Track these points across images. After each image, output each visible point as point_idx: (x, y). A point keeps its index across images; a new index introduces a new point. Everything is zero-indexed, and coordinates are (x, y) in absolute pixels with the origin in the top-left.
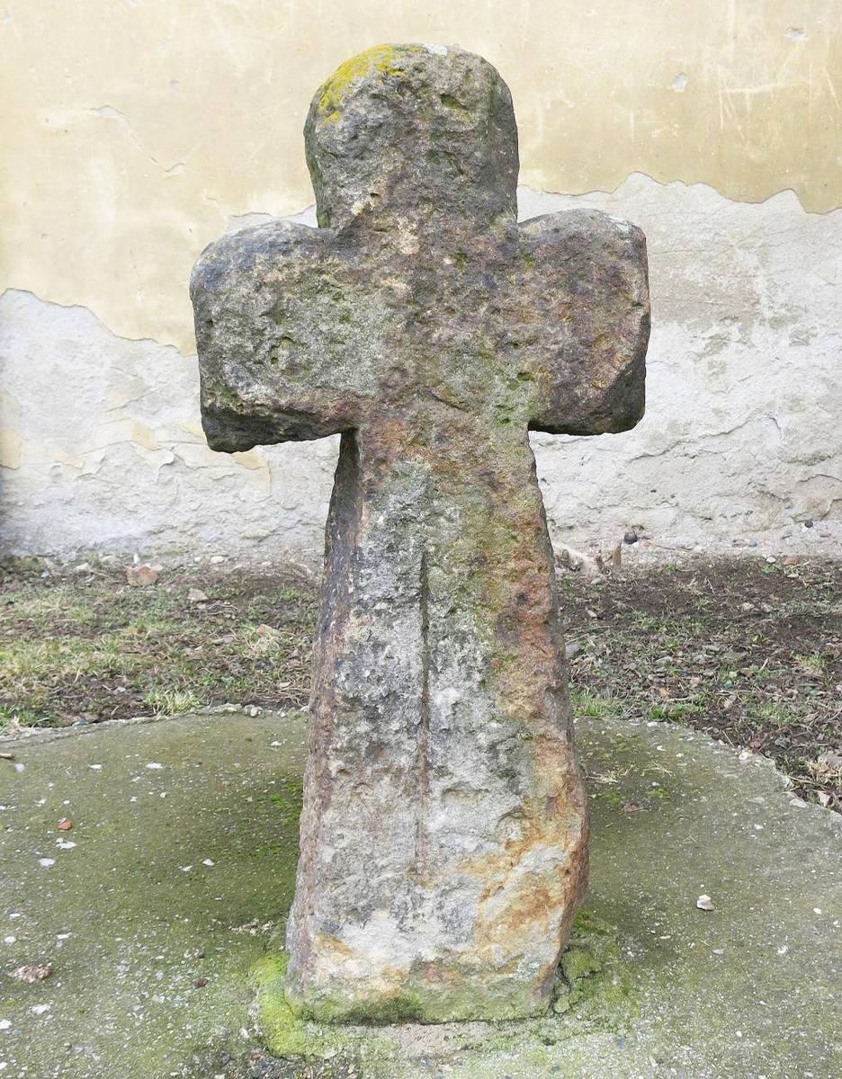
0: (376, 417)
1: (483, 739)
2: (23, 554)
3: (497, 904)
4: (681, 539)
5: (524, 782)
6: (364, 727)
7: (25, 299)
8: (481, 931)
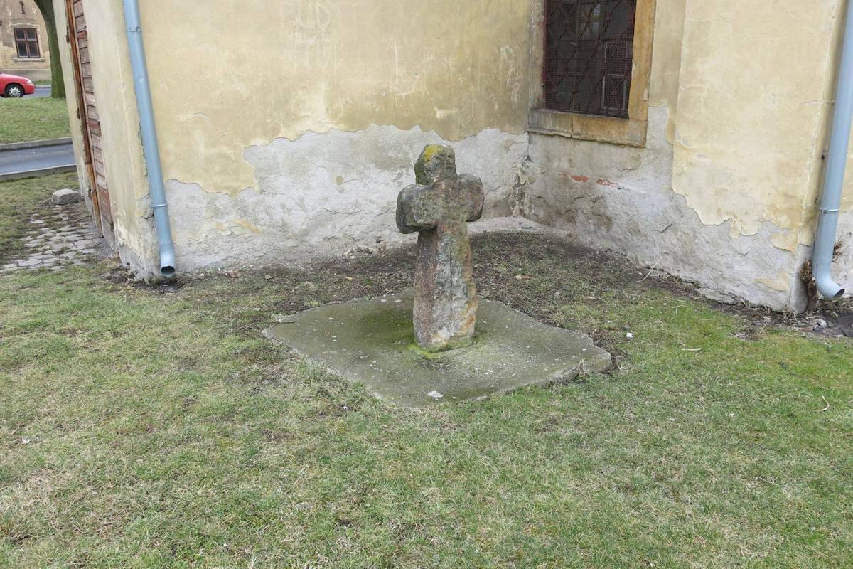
0: (442, 223)
1: (462, 287)
2: (179, 273)
3: (464, 322)
4: (393, 240)
5: (469, 295)
6: (440, 288)
7: (174, 182)
8: (462, 328)
